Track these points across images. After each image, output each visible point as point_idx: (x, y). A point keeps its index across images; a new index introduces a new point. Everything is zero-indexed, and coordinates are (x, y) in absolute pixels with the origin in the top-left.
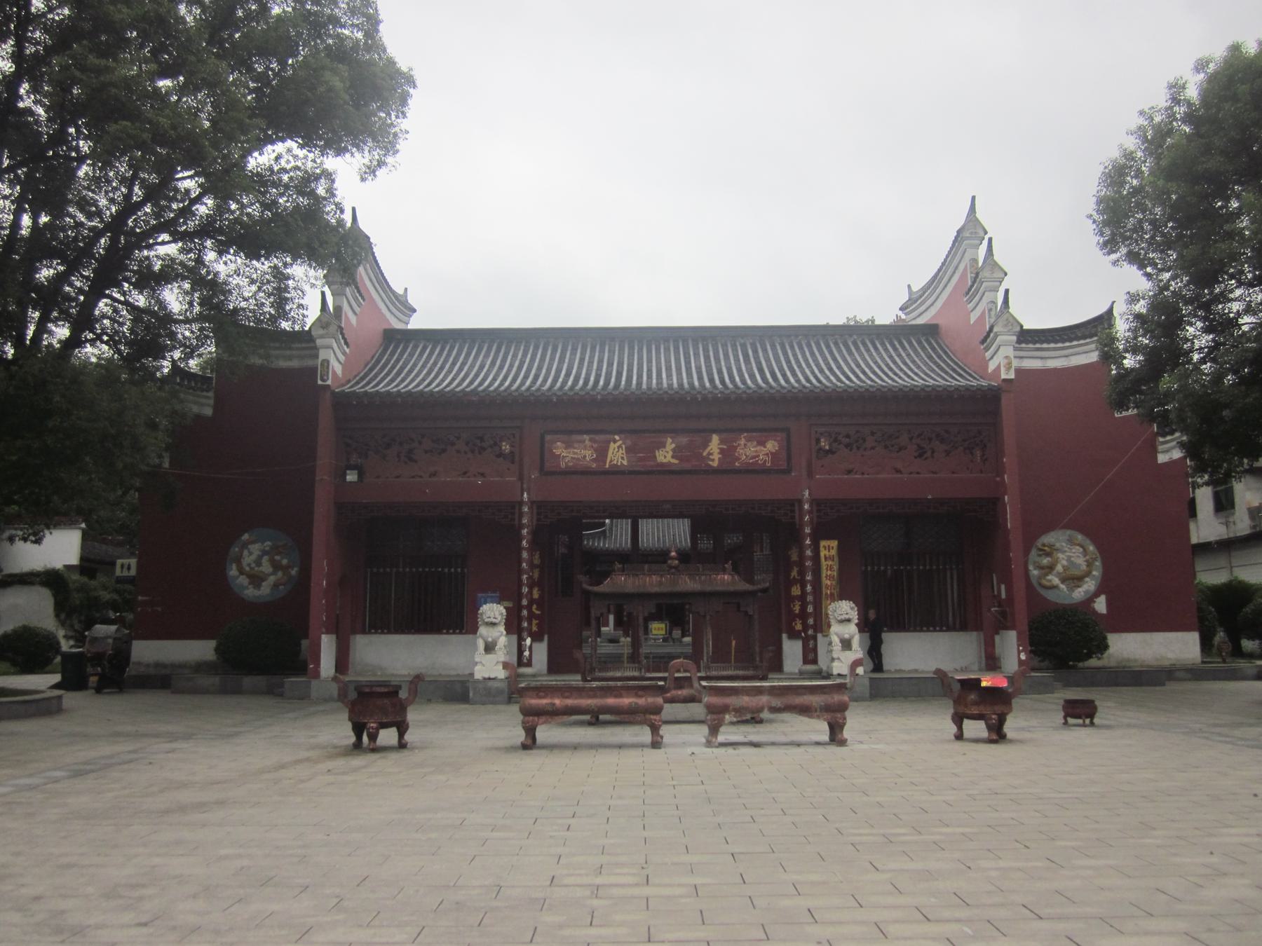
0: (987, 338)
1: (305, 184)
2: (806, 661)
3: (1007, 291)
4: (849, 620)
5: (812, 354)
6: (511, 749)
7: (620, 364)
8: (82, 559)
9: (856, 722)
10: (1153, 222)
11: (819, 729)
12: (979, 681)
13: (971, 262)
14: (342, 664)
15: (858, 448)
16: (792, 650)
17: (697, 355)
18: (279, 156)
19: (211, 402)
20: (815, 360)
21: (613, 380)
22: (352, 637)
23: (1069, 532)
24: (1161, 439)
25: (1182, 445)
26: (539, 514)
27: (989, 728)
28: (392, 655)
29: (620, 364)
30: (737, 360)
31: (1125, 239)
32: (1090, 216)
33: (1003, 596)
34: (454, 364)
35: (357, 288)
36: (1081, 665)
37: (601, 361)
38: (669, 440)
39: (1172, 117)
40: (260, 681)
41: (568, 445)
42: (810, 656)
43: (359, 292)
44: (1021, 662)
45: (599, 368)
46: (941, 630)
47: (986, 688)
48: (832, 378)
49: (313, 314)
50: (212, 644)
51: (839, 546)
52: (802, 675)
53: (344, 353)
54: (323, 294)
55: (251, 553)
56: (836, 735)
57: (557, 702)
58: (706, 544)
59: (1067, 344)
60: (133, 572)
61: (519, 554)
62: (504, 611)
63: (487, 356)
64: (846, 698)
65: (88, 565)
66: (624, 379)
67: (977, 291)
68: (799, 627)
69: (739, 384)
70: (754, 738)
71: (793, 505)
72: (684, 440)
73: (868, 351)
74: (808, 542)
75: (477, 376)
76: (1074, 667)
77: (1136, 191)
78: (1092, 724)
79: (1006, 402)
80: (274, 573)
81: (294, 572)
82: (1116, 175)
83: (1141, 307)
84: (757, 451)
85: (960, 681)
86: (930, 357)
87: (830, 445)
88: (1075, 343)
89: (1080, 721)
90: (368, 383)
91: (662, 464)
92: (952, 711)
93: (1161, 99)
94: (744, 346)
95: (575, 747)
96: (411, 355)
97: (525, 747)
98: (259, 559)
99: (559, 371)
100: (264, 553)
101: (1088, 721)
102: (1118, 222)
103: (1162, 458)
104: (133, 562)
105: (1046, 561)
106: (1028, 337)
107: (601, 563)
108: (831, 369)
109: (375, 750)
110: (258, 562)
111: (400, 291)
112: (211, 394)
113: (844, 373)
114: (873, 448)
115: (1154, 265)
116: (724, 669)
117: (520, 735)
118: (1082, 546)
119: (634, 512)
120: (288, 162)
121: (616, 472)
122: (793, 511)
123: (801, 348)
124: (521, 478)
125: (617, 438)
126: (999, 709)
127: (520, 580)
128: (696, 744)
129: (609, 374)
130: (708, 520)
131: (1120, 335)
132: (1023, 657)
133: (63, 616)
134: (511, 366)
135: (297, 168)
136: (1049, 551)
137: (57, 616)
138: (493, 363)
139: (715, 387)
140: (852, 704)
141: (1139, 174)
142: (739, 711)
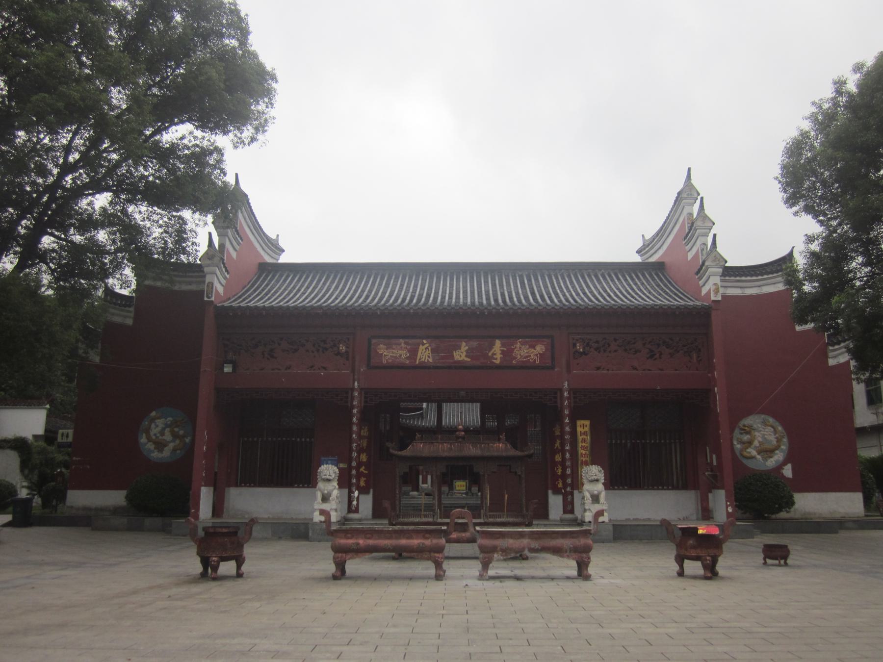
0: (700, 270)
1: (201, 156)
2: (565, 511)
3: (715, 236)
4: (597, 480)
5: (571, 283)
6: (325, 579)
7: (430, 288)
8: (46, 431)
9: (597, 562)
10: (824, 183)
11: (569, 567)
12: (696, 529)
13: (688, 217)
14: (218, 509)
15: (605, 351)
16: (555, 502)
17: (486, 282)
18: (181, 133)
19: (132, 315)
20: (574, 287)
21: (423, 299)
22: (227, 489)
23: (763, 416)
24: (831, 348)
25: (849, 351)
26: (365, 398)
27: (705, 567)
28: (253, 502)
29: (430, 288)
30: (516, 286)
31: (803, 196)
32: (776, 178)
33: (715, 463)
34: (308, 288)
35: (237, 231)
36: (773, 516)
37: (416, 286)
38: (464, 344)
39: (836, 104)
40: (158, 521)
41: (389, 347)
42: (568, 507)
43: (238, 234)
44: (728, 514)
45: (414, 291)
46: (668, 489)
47: (702, 535)
48: (586, 299)
49: (203, 249)
50: (124, 493)
51: (591, 425)
52: (563, 523)
53: (225, 278)
54: (210, 234)
55: (157, 426)
56: (583, 573)
57: (361, 542)
58: (492, 423)
59: (760, 277)
60: (70, 439)
61: (351, 428)
62: (337, 471)
63: (332, 282)
64: (590, 542)
65: (49, 436)
66: (431, 299)
67: (693, 236)
68: (560, 485)
69: (516, 302)
70: (518, 573)
71: (556, 393)
72: (474, 344)
73: (612, 280)
74: (567, 421)
75: (324, 296)
76: (765, 518)
77: (809, 161)
78: (786, 564)
79: (716, 320)
80: (173, 441)
81: (187, 440)
82: (796, 148)
83: (815, 247)
84: (528, 352)
85: (681, 529)
86: (658, 286)
87: (584, 348)
88: (766, 276)
89: (777, 562)
90: (244, 300)
91: (459, 362)
92: (674, 553)
93: (828, 92)
94: (521, 277)
95: (374, 579)
96: (278, 281)
97: (335, 578)
98: (164, 429)
99: (384, 293)
100: (167, 426)
101: (782, 562)
102: (800, 180)
103: (832, 362)
104: (71, 432)
105: (746, 438)
106: (731, 272)
107: (409, 435)
108: (585, 293)
109: (215, 579)
110: (162, 433)
111: (274, 237)
112: (132, 309)
113: (594, 296)
114: (615, 351)
115: (825, 215)
116: (500, 517)
117: (332, 568)
118: (773, 427)
119: (440, 397)
120: (190, 141)
121: (423, 367)
122: (556, 398)
123: (563, 278)
124: (353, 371)
125: (425, 341)
126: (712, 552)
127: (351, 448)
128: (471, 578)
129: (421, 296)
130: (492, 404)
131: (800, 267)
132: (730, 510)
133: (26, 472)
134: (350, 289)
135: (197, 146)
136: (748, 430)
137: (22, 471)
138: (337, 287)
139: (498, 305)
140: (595, 546)
141: (812, 147)
142: (505, 551)
